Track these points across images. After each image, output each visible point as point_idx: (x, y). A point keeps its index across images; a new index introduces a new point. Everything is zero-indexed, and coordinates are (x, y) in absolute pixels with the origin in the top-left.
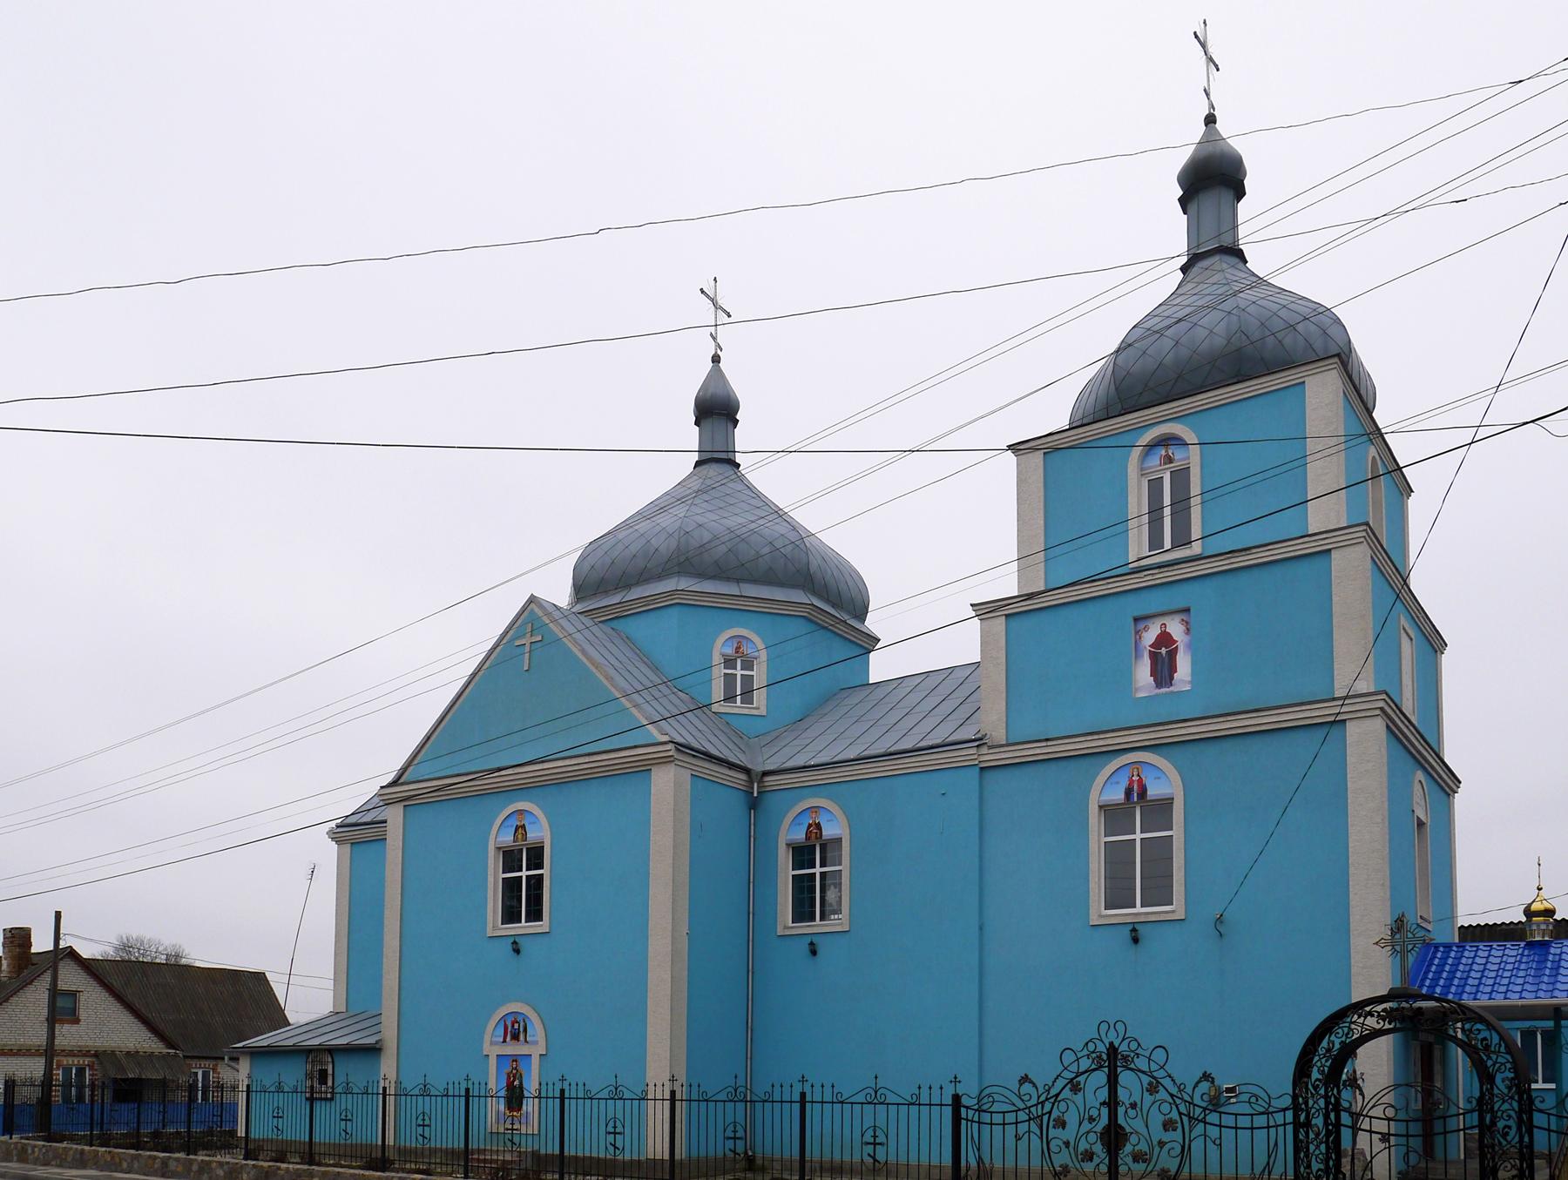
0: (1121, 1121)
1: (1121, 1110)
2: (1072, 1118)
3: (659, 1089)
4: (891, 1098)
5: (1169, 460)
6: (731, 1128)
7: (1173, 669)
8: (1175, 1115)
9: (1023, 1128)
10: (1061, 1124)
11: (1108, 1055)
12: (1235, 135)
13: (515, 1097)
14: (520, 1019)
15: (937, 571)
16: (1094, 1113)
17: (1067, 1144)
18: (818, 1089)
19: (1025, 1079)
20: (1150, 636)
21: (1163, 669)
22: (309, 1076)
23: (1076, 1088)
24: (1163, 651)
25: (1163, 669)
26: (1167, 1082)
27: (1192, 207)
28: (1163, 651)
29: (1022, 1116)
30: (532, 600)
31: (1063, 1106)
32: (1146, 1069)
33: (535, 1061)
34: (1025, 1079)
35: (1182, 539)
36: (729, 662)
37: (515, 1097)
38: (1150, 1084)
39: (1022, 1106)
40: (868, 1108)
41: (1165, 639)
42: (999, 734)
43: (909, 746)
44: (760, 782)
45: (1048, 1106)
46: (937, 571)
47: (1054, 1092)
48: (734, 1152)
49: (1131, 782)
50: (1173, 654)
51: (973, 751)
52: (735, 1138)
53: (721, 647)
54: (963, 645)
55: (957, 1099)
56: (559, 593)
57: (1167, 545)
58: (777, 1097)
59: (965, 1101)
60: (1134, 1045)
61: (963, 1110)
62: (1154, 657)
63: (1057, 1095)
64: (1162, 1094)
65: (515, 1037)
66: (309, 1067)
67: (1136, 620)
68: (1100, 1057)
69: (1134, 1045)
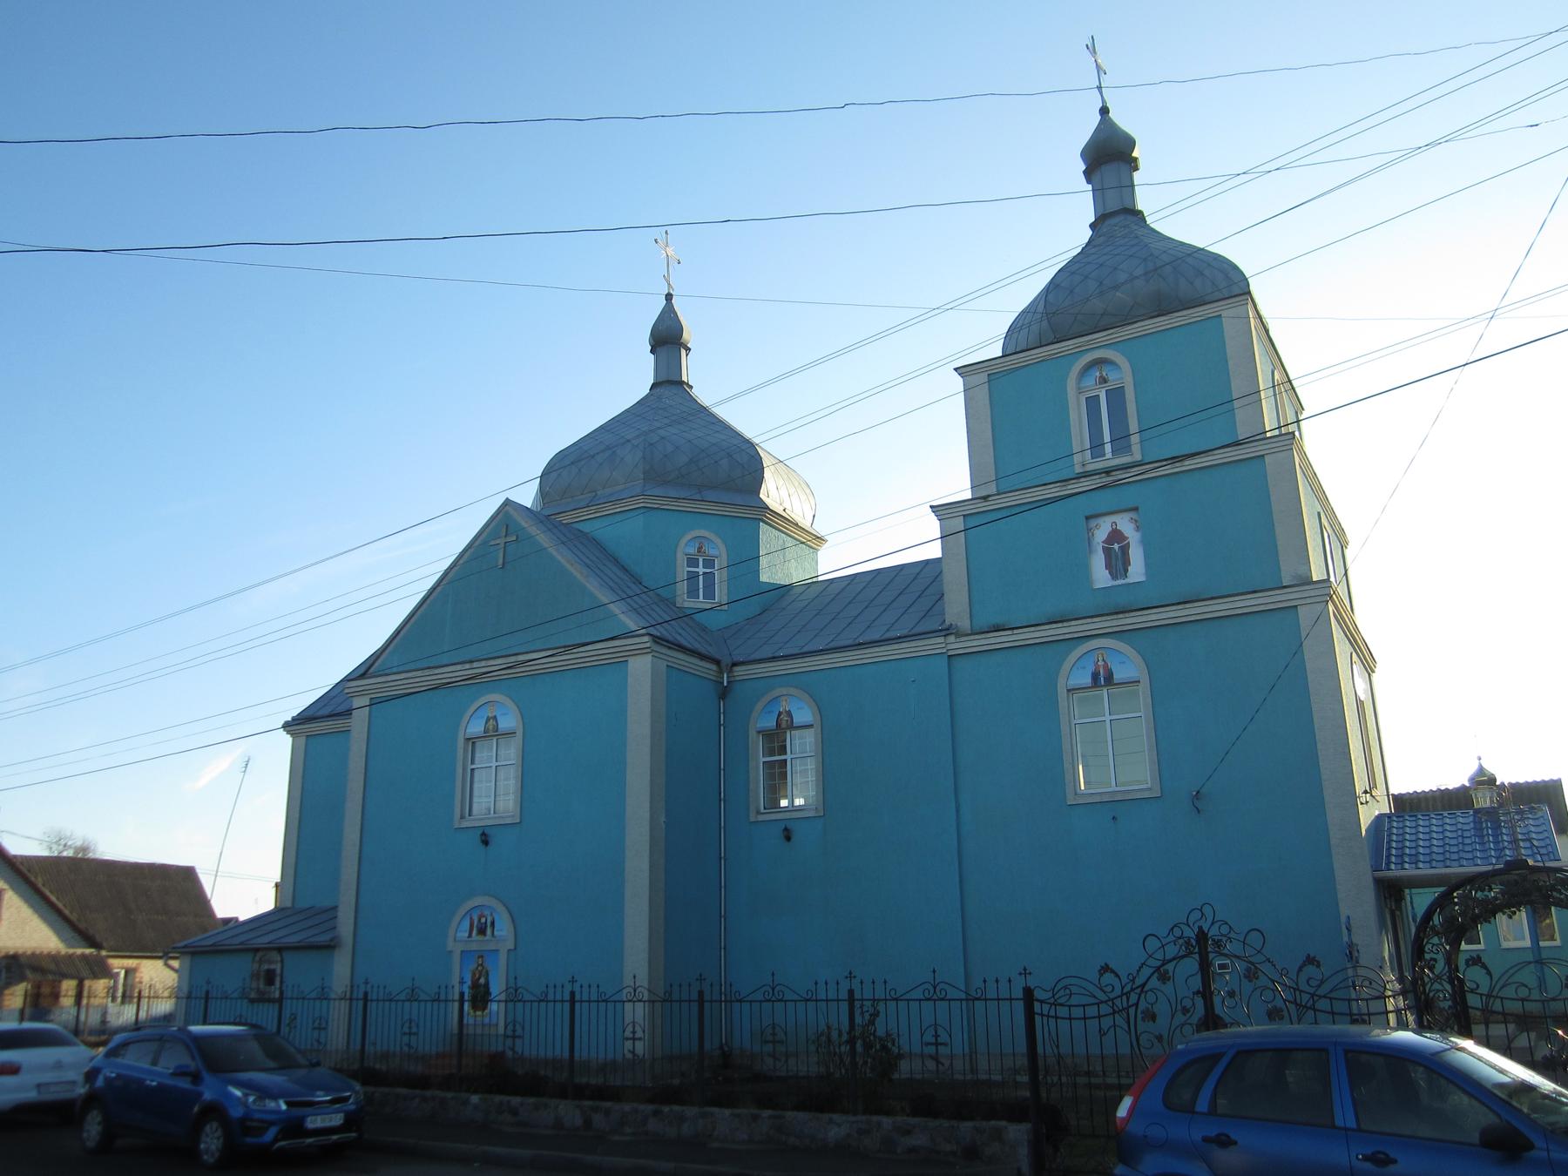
0: (1218, 1010)
1: (1217, 1000)
2: (1162, 1009)
3: (559, 990)
4: (527, 997)
5: (1104, 380)
6: (630, 1028)
7: (1126, 562)
8: (1279, 1003)
9: (1107, 1022)
10: (1153, 1018)
11: (1198, 942)
12: (1123, 119)
14: (487, 912)
15: (868, 479)
16: (1187, 1003)
17: (1160, 1038)
18: (585, 990)
19: (1105, 969)
20: (1102, 532)
21: (1117, 561)
22: (255, 976)
23: (1164, 978)
24: (1116, 546)
25: (1117, 561)
26: (1266, 968)
27: (1096, 177)
28: (1116, 546)
30: (507, 502)
31: (1151, 997)
33: (503, 957)
34: (1105, 969)
35: (1121, 440)
36: (692, 562)
37: (480, 997)
38: (1248, 970)
39: (1104, 998)
40: (407, 1004)
41: (1116, 536)
42: (965, 624)
43: (876, 637)
44: (730, 671)
45: (1133, 998)
46: (868, 479)
47: (1139, 982)
48: (633, 1052)
50: (1125, 550)
51: (941, 640)
53: (685, 548)
54: (919, 541)
55: (1028, 994)
56: (527, 496)
57: (1109, 455)
58: (992, 994)
59: (1038, 994)
60: (1225, 929)
61: (1037, 1006)
63: (1143, 985)
64: (1263, 981)
65: (482, 931)
66: (256, 966)
67: (1087, 518)
68: (1188, 943)
69: (1225, 929)
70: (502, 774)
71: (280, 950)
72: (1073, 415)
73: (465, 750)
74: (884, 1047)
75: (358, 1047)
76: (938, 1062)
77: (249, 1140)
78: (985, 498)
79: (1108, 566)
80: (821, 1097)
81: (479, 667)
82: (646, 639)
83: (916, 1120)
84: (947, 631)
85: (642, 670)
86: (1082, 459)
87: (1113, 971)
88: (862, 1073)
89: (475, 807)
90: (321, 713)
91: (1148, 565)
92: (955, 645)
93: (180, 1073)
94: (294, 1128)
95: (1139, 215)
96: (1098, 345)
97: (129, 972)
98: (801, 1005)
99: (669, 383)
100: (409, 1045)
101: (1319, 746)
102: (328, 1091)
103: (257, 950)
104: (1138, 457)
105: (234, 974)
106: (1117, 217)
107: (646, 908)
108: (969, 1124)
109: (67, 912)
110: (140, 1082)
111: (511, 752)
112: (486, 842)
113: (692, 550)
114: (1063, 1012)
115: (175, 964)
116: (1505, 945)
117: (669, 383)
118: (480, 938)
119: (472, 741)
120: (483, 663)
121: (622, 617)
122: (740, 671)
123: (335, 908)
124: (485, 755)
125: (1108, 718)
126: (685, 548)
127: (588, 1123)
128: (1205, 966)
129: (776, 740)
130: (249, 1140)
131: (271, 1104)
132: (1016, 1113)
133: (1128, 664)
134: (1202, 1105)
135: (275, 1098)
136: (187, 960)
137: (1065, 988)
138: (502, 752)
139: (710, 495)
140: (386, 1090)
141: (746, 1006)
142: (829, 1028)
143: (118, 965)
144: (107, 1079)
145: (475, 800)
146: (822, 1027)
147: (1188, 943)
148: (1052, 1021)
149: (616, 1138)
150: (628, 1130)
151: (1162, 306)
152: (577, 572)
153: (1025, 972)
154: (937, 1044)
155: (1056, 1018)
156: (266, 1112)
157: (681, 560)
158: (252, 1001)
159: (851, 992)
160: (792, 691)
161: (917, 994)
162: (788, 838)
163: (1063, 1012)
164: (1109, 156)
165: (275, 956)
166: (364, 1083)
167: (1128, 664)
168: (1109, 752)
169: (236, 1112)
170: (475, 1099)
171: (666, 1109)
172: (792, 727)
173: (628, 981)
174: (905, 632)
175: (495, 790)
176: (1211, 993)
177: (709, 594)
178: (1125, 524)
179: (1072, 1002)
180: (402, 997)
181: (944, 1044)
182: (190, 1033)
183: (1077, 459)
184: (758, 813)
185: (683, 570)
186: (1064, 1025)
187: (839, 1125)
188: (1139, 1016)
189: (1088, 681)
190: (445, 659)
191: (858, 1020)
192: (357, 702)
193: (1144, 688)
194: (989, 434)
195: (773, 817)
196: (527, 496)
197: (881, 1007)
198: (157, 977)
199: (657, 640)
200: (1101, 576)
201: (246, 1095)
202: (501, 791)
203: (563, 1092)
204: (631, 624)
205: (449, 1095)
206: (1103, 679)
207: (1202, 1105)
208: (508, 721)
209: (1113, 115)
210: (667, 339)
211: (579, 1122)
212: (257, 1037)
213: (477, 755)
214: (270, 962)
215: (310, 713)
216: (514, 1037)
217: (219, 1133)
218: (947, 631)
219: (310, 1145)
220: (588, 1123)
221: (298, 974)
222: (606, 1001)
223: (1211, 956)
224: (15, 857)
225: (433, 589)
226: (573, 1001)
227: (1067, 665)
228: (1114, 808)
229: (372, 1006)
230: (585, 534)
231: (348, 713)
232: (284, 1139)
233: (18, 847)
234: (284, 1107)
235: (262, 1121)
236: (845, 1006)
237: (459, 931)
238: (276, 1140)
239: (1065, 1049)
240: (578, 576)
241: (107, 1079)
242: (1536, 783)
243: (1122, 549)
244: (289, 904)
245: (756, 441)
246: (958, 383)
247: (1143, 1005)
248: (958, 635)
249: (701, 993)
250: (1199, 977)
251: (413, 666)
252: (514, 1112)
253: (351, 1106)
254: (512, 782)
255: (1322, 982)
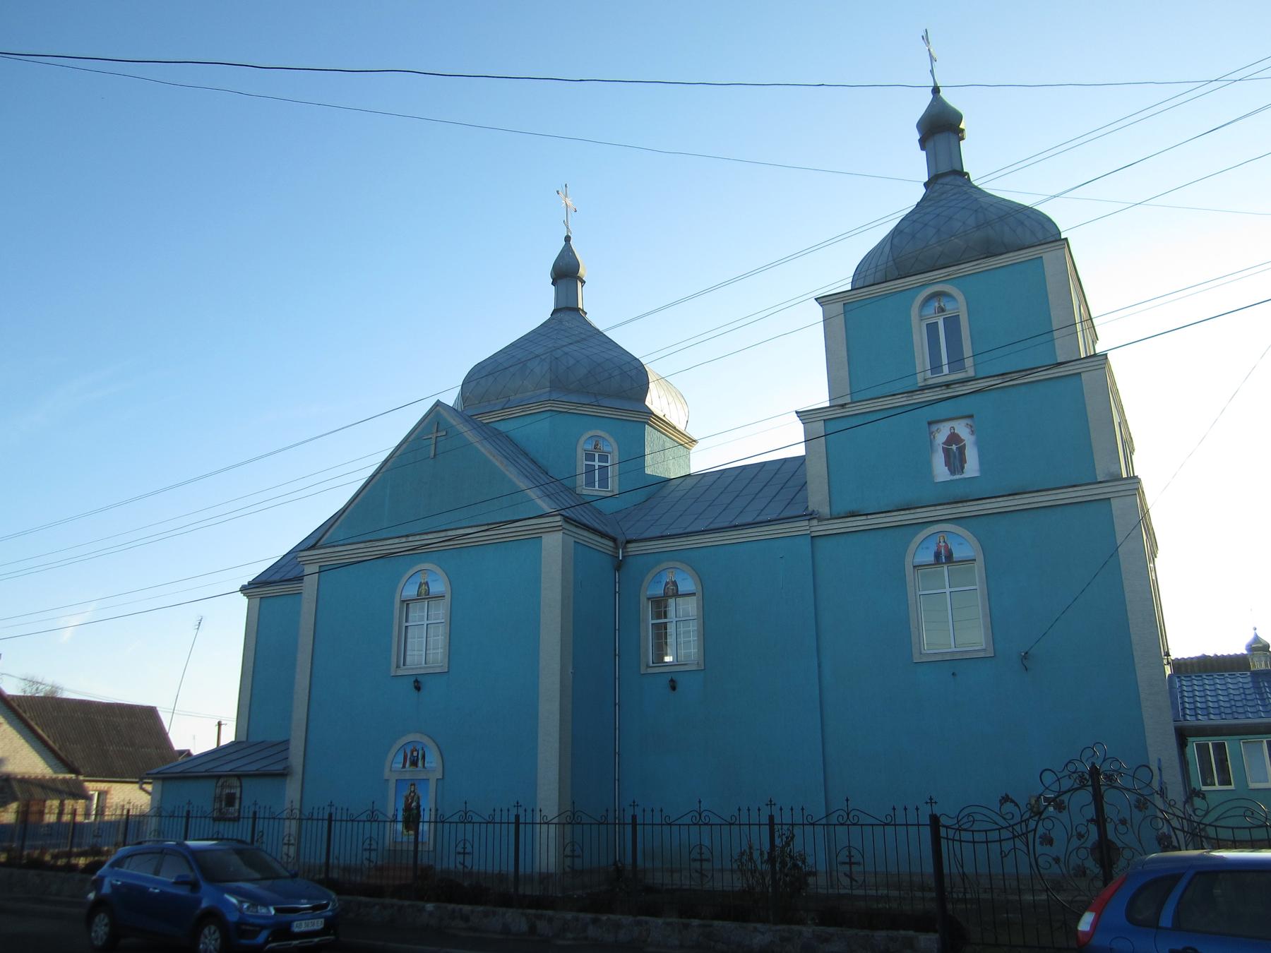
0: (1111, 835)
1: (1110, 828)
4: (381, 818)
5: (942, 310)
6: (461, 845)
7: (963, 460)
9: (1007, 846)
10: (1050, 842)
12: (951, 98)
13: (412, 818)
15: (738, 390)
16: (1083, 830)
17: (1057, 860)
18: (339, 811)
19: (1006, 799)
21: (955, 459)
22: (218, 799)
24: (954, 447)
25: (955, 459)
27: (930, 144)
28: (954, 447)
29: (1006, 834)
30: (438, 403)
32: (1129, 786)
34: (1006, 799)
35: (957, 361)
36: (590, 457)
37: (412, 818)
38: (1138, 801)
39: (1005, 824)
41: (954, 438)
42: (825, 510)
43: (750, 520)
44: (624, 548)
45: (1032, 824)
46: (738, 390)
49: (939, 547)
50: (962, 450)
51: (806, 523)
52: (370, 850)
53: (584, 445)
54: (785, 440)
55: (935, 821)
56: (450, 399)
58: (497, 820)
59: (943, 820)
61: (943, 832)
62: (947, 452)
65: (414, 763)
67: (930, 423)
70: (431, 631)
71: (239, 777)
72: (916, 337)
73: (401, 612)
74: (795, 866)
75: (323, 860)
76: (852, 879)
77: (244, 941)
78: (843, 406)
79: (947, 463)
80: (738, 908)
81: (416, 541)
82: (558, 518)
83: (831, 930)
84: (811, 516)
85: (554, 545)
86: (923, 374)
87: (1012, 801)
88: (779, 889)
89: (408, 659)
90: (272, 579)
91: (981, 463)
92: (818, 528)
93: (179, 883)
94: (282, 931)
95: (962, 174)
96: (937, 281)
97: (102, 794)
98: (726, 829)
99: (567, 309)
100: (369, 860)
101: (1129, 615)
102: (309, 898)
103: (219, 777)
104: (971, 373)
105: (203, 797)
106: (947, 177)
107: (557, 745)
108: (883, 933)
109: (51, 743)
110: (143, 891)
111: (440, 612)
112: (418, 688)
113: (590, 447)
114: (966, 836)
115: (149, 788)
116: (1252, 785)
117: (567, 309)
118: (412, 768)
119: (406, 603)
120: (418, 538)
121: (539, 502)
122: (631, 547)
123: (287, 742)
124: (417, 614)
125: (948, 590)
126: (584, 445)
127: (533, 929)
128: (1098, 798)
129: (660, 606)
130: (244, 941)
131: (263, 911)
132: (922, 923)
133: (965, 546)
134: (1166, 920)
135: (266, 905)
136: (159, 784)
137: (969, 815)
138: (432, 612)
139: (606, 402)
140: (349, 898)
141: (675, 828)
142: (751, 848)
143: (93, 788)
144: (113, 886)
145: (408, 653)
146: (745, 847)
147: (1082, 778)
148: (957, 844)
149: (560, 942)
150: (569, 935)
151: (990, 249)
152: (498, 462)
153: (931, 801)
154: (851, 864)
155: (961, 841)
156: (263, 917)
157: (581, 455)
158: (215, 820)
159: (771, 817)
160: (678, 565)
161: (687, 820)
162: (674, 688)
163: (966, 836)
164: (940, 128)
165: (235, 782)
166: (339, 893)
167: (965, 546)
168: (951, 621)
169: (233, 917)
170: (430, 907)
171: (604, 918)
172: (676, 595)
173: (287, 805)
174: (774, 516)
175: (425, 643)
176: (1105, 821)
177: (604, 482)
178: (962, 429)
179: (975, 827)
180: (456, 818)
181: (858, 864)
182: (187, 847)
183: (920, 377)
184: (648, 666)
185: (582, 464)
186: (968, 848)
187: (763, 933)
188: (1038, 841)
189: (931, 559)
190: (384, 534)
191: (778, 841)
192: (309, 569)
193: (979, 566)
194: (845, 353)
195: (662, 670)
196: (450, 399)
197: (797, 830)
198: (128, 797)
199: (567, 519)
200: (941, 471)
201: (241, 902)
202: (431, 645)
203: (507, 901)
204: (546, 506)
205: (407, 903)
206: (944, 557)
207: (1166, 920)
208: (439, 586)
209: (944, 94)
210: (566, 273)
211: (524, 927)
212: (239, 852)
213: (411, 615)
214: (230, 787)
215: (264, 579)
216: (370, 850)
217: (217, 935)
218: (811, 516)
219: (295, 946)
220: (533, 929)
221: (253, 795)
222: (547, 823)
223: (1103, 788)
224: (14, 697)
225: (373, 476)
226: (517, 823)
227: (913, 546)
228: (954, 665)
229: (336, 826)
230: (500, 433)
231: (299, 579)
232: (273, 941)
233: (12, 689)
234: (273, 912)
235: (252, 925)
236: (766, 829)
237: (394, 765)
238: (267, 942)
239: (969, 869)
240: (497, 464)
241: (113, 886)
242: (1230, 656)
243: (959, 450)
244: (244, 739)
245: (643, 361)
246: (818, 311)
247: (1040, 831)
248: (820, 519)
249: (517, 817)
250: (1093, 806)
251: (355, 540)
252: (466, 918)
253: (328, 912)
254: (441, 638)
255: (1207, 812)
